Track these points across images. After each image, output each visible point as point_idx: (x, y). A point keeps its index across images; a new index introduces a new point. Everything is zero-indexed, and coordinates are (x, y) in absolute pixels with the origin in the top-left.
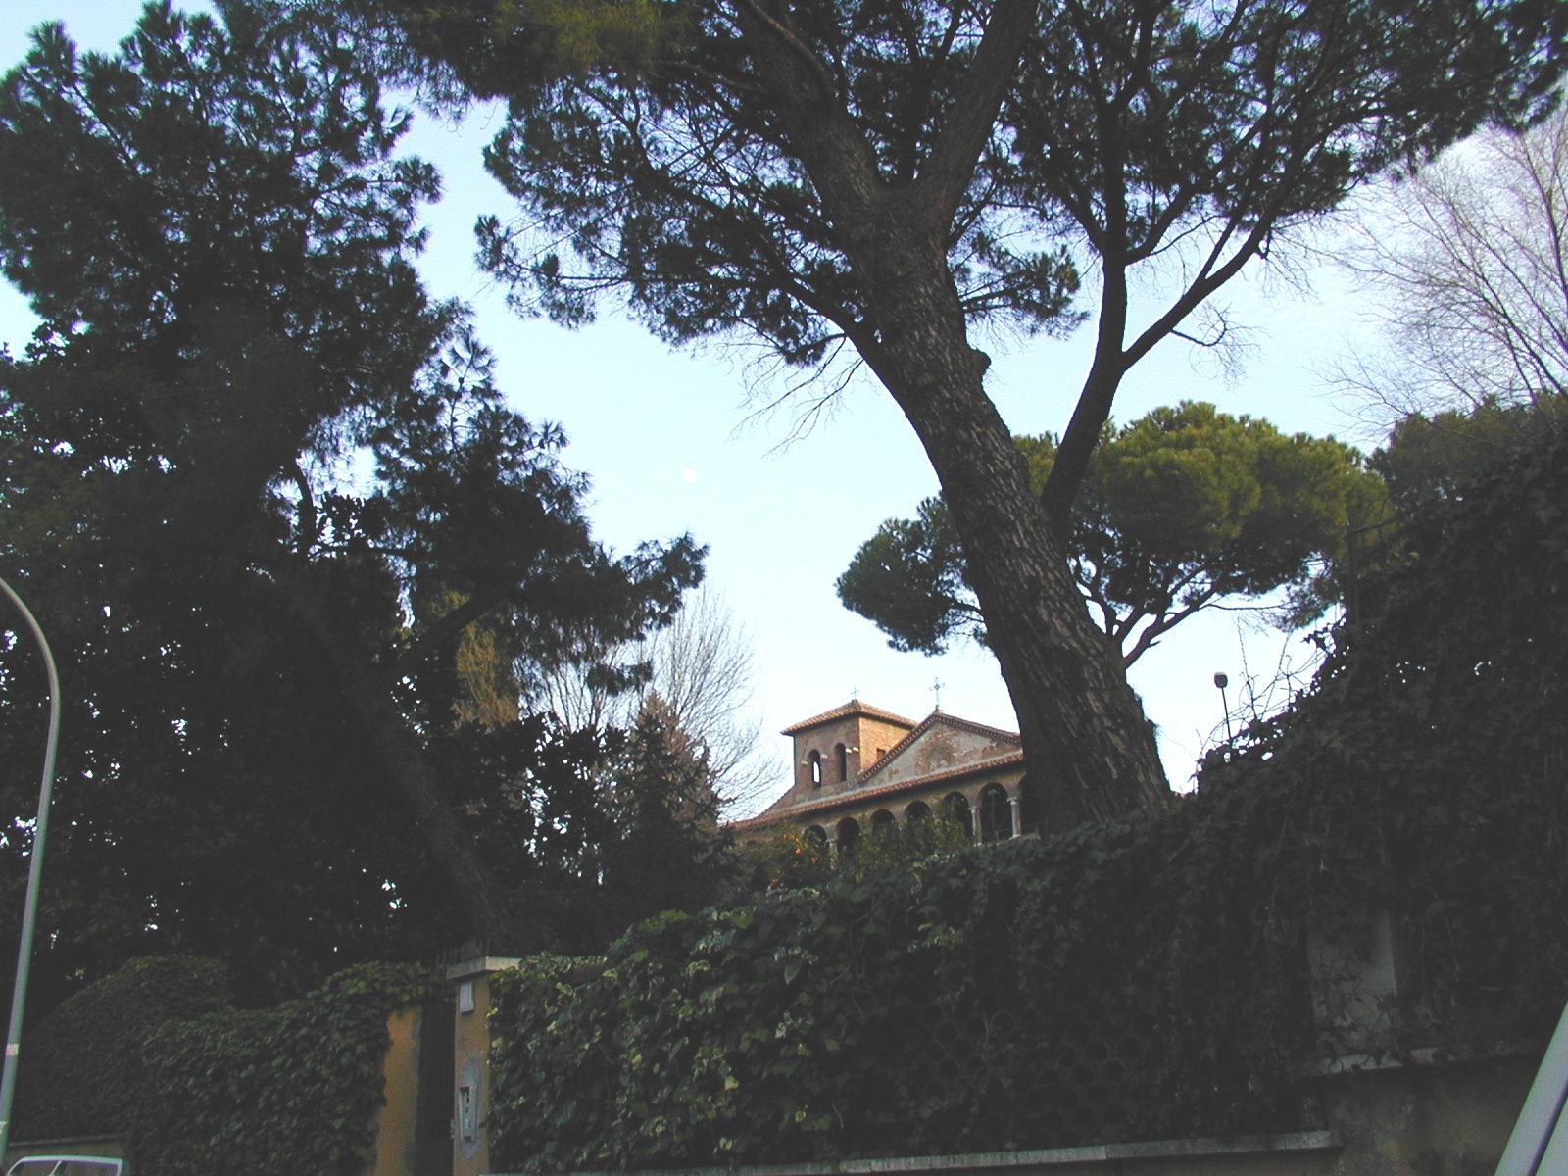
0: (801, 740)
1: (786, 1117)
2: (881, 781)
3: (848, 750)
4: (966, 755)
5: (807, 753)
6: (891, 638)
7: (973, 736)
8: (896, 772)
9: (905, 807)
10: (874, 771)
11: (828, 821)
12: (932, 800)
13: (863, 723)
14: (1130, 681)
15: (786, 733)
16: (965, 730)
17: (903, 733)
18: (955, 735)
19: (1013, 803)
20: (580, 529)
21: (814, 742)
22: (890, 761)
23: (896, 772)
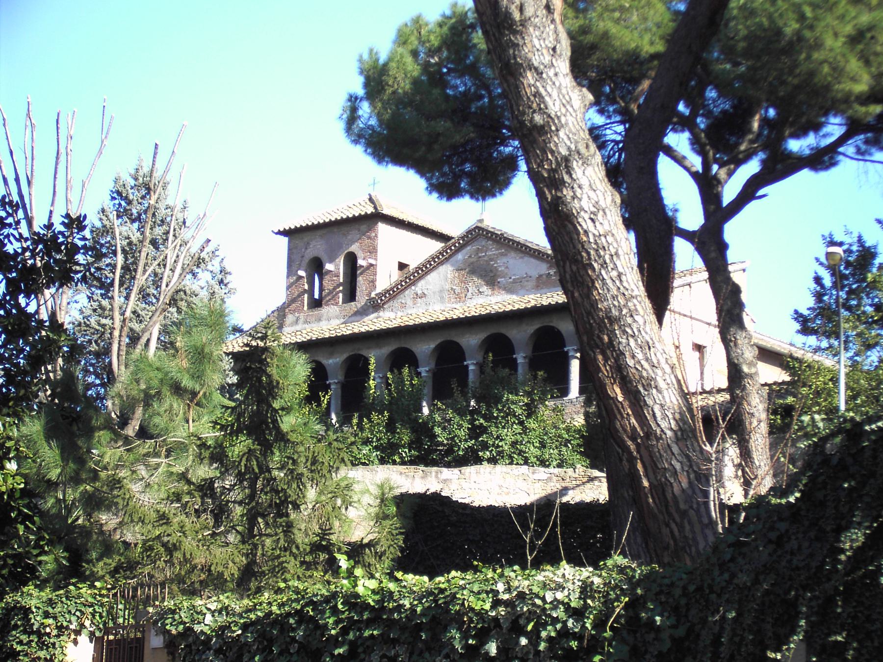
0: (299, 242)
1: (558, 502)
2: (404, 306)
3: (361, 262)
4: (515, 281)
5: (306, 260)
6: (360, 92)
7: (526, 259)
8: (424, 295)
9: (433, 346)
10: (393, 293)
11: (331, 355)
12: (471, 341)
13: (382, 228)
14: (701, 221)
15: (279, 233)
16: (516, 250)
17: (436, 246)
18: (502, 254)
19: (471, 368)
20: (421, 172)
21: (316, 247)
22: (414, 283)
23: (424, 295)
